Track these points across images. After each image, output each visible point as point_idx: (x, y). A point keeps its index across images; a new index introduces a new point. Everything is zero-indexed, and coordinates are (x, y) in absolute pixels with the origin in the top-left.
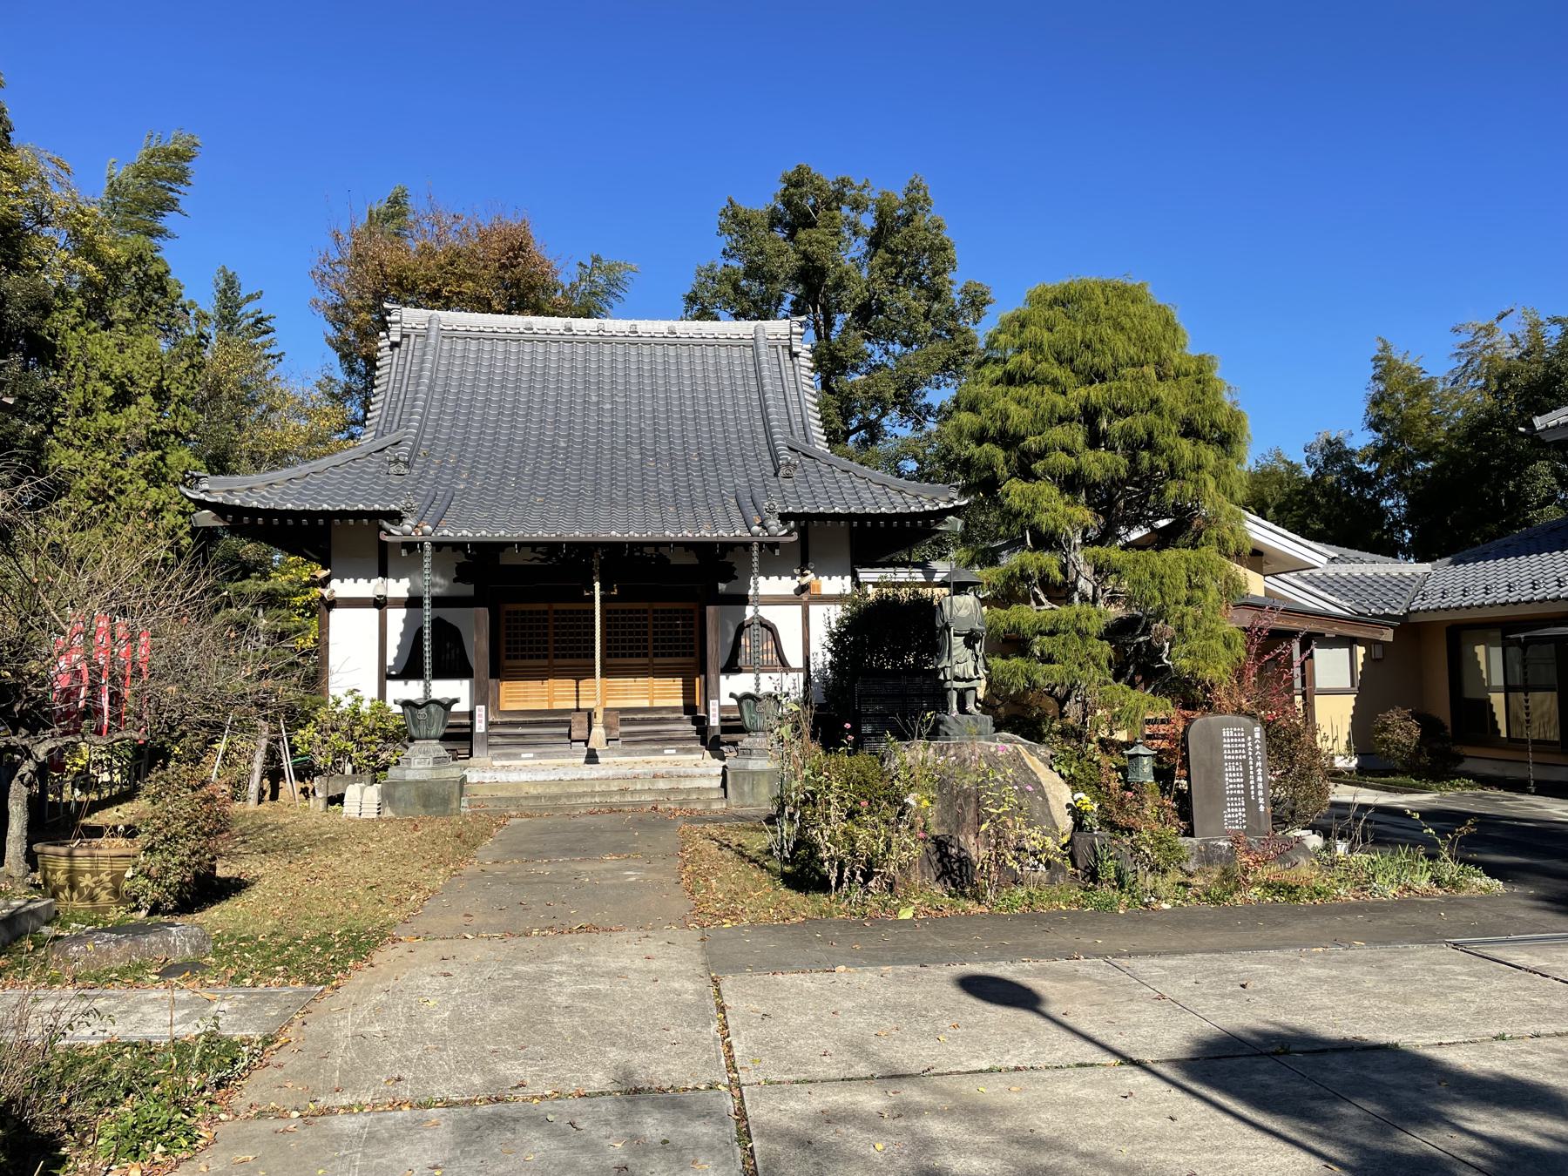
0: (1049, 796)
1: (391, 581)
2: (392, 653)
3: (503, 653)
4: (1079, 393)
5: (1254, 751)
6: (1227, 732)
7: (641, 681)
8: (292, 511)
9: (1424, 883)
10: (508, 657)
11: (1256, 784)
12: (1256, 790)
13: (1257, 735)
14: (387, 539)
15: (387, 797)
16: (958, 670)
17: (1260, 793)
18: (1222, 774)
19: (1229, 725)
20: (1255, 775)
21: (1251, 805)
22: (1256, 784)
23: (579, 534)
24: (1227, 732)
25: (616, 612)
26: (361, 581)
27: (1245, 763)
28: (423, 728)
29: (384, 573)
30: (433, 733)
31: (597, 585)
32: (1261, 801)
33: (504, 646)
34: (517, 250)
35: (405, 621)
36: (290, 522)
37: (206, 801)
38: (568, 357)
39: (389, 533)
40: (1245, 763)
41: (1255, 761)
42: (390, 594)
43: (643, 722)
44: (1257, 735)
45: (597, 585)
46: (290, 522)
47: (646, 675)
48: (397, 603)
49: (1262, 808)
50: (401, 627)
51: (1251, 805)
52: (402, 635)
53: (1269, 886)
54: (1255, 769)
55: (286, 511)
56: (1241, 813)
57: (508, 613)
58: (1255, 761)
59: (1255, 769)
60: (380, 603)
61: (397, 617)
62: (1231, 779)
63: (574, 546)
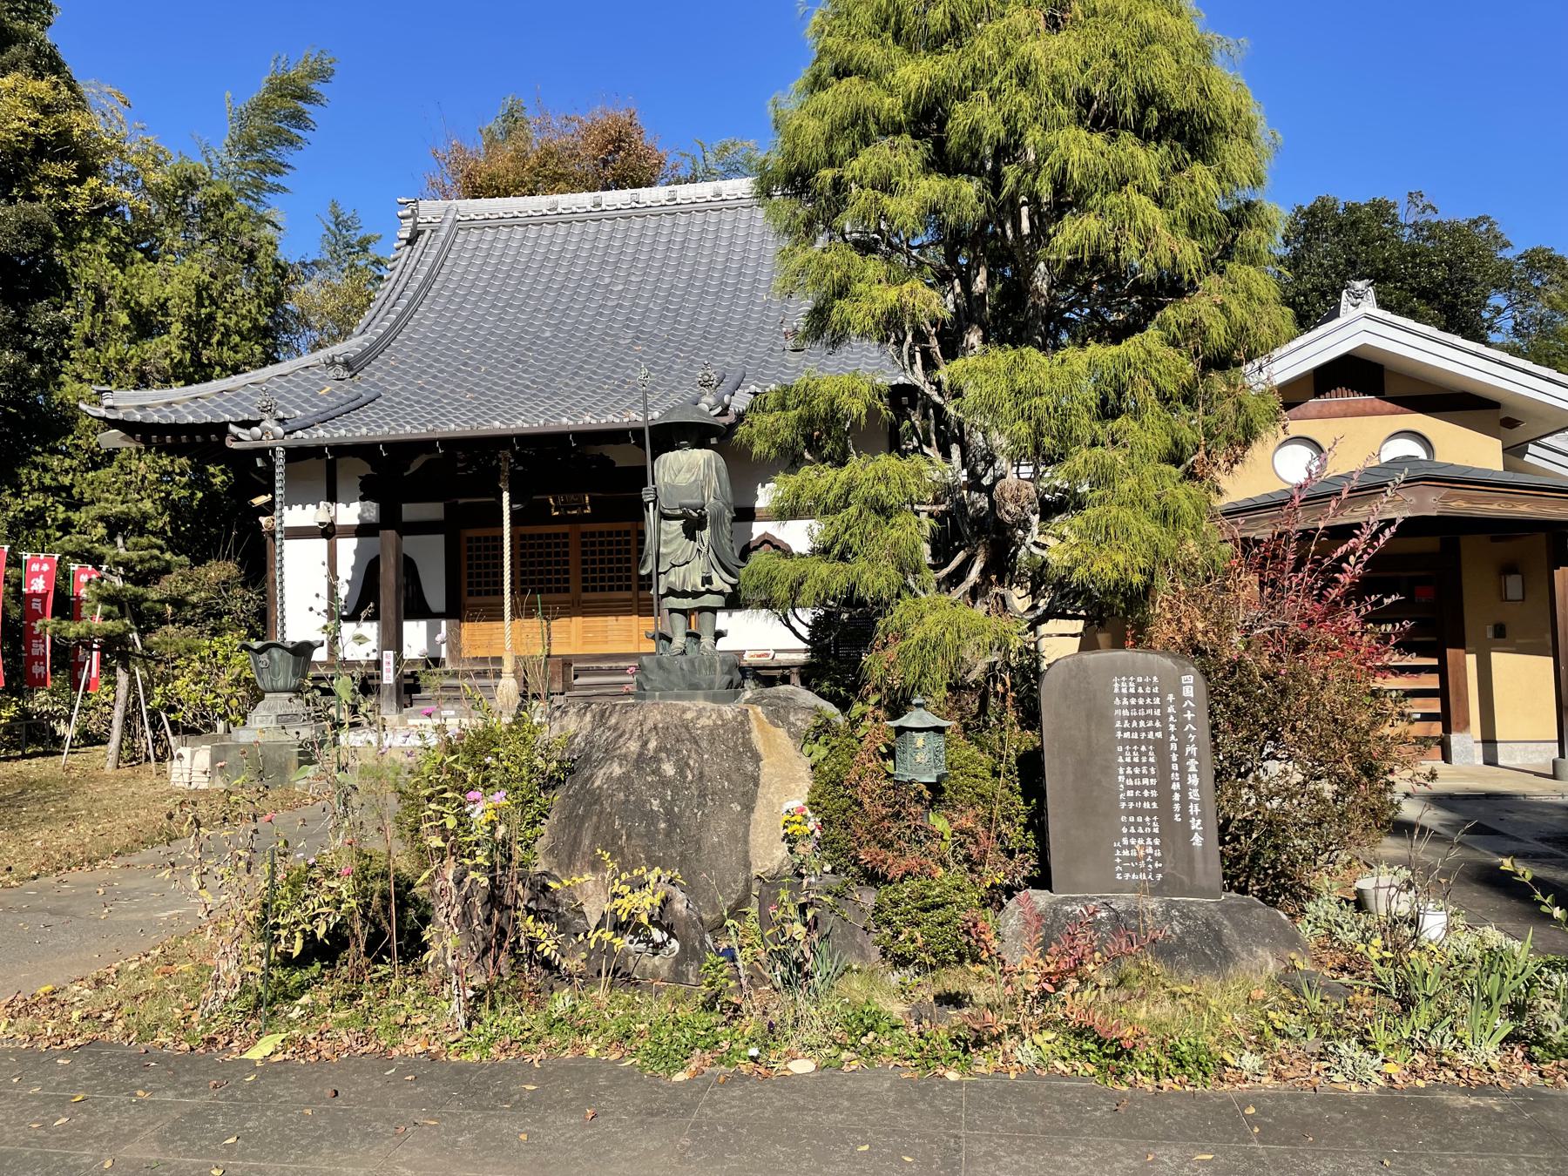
0: (760, 804)
1: (341, 506)
2: (343, 591)
3: (465, 589)
4: (916, 73)
5: (1181, 724)
6: (1121, 686)
7: (611, 620)
8: (159, 424)
9: (1489, 1051)
10: (470, 594)
11: (1184, 791)
12: (1185, 802)
13: (1188, 692)
14: (235, 445)
15: (217, 766)
16: (674, 579)
17: (1194, 809)
18: (1109, 769)
19: (1126, 671)
20: (1183, 772)
21: (1173, 834)
22: (1184, 791)
23: (454, 426)
24: (1121, 686)
25: (593, 534)
26: (309, 507)
27: (1161, 747)
28: (267, 677)
29: (332, 498)
30: (280, 683)
31: (506, 496)
32: (1196, 824)
33: (465, 581)
34: (617, 141)
35: (357, 552)
36: (198, 438)
37: (712, 742)
38: (591, 237)
39: (239, 440)
40: (1161, 747)
41: (1182, 746)
42: (340, 522)
43: (599, 672)
44: (1188, 692)
45: (506, 496)
46: (198, 438)
47: (629, 613)
48: (348, 531)
49: (1197, 840)
50: (351, 560)
51: (1173, 834)
52: (353, 568)
53: (1079, 1034)
54: (1182, 759)
55: (135, 423)
56: (1146, 847)
57: (470, 540)
58: (1182, 746)
59: (1182, 759)
60: (328, 531)
61: (347, 548)
62: (1130, 776)
63: (452, 444)
